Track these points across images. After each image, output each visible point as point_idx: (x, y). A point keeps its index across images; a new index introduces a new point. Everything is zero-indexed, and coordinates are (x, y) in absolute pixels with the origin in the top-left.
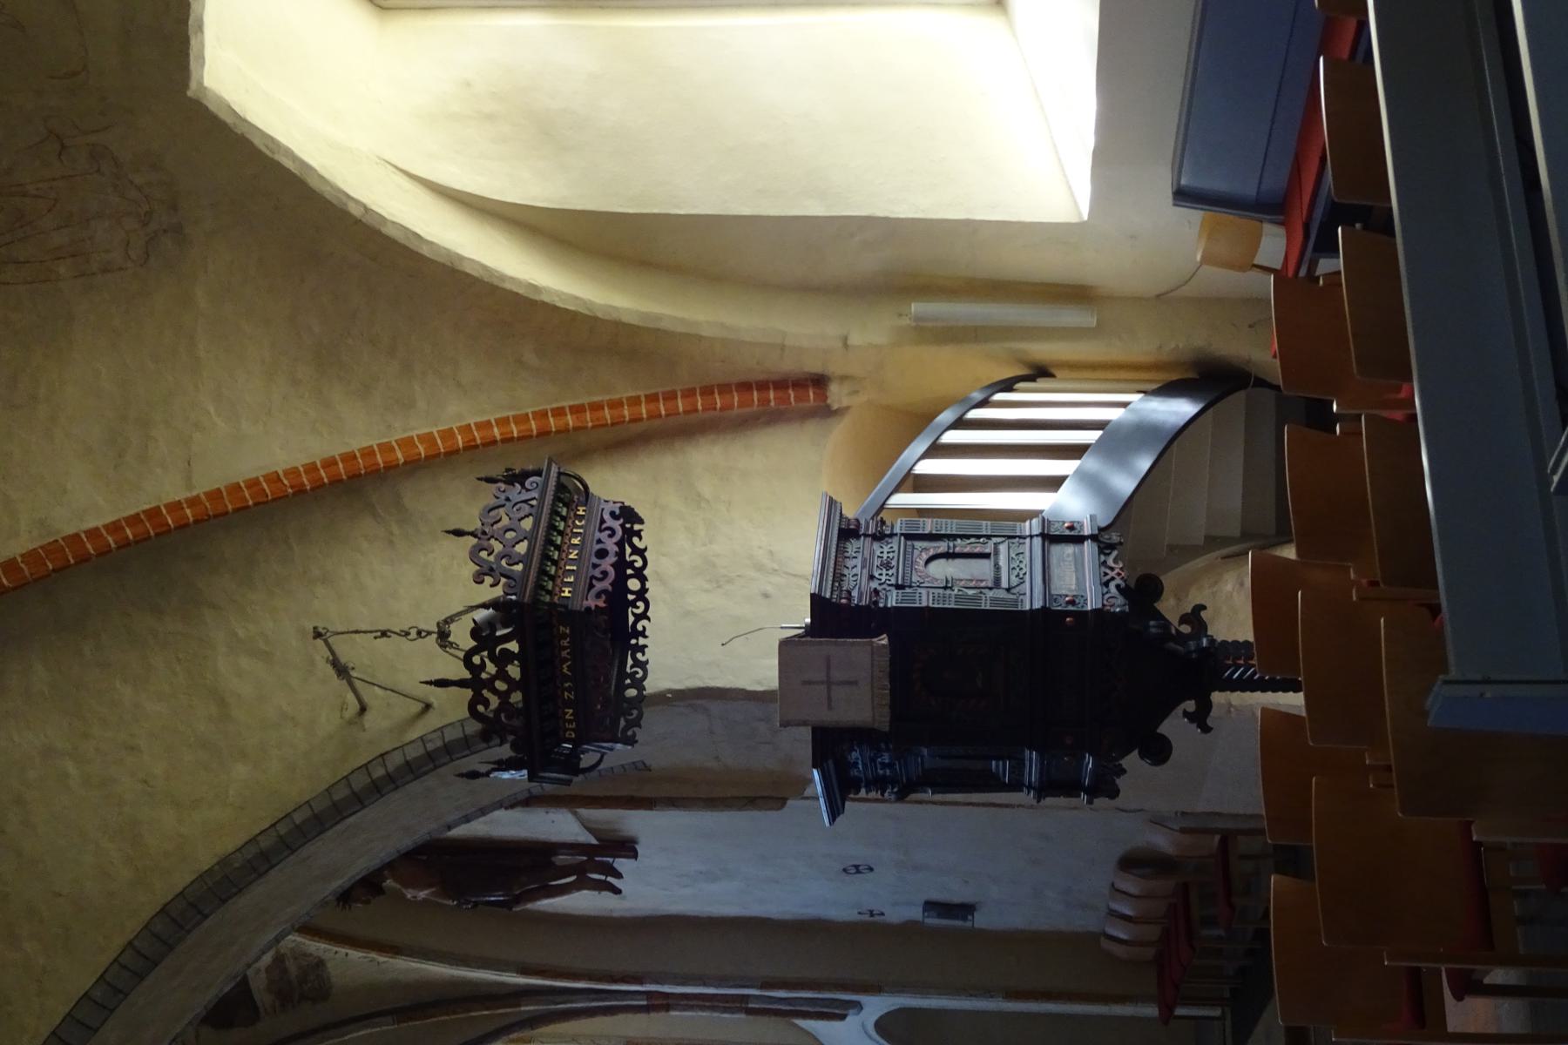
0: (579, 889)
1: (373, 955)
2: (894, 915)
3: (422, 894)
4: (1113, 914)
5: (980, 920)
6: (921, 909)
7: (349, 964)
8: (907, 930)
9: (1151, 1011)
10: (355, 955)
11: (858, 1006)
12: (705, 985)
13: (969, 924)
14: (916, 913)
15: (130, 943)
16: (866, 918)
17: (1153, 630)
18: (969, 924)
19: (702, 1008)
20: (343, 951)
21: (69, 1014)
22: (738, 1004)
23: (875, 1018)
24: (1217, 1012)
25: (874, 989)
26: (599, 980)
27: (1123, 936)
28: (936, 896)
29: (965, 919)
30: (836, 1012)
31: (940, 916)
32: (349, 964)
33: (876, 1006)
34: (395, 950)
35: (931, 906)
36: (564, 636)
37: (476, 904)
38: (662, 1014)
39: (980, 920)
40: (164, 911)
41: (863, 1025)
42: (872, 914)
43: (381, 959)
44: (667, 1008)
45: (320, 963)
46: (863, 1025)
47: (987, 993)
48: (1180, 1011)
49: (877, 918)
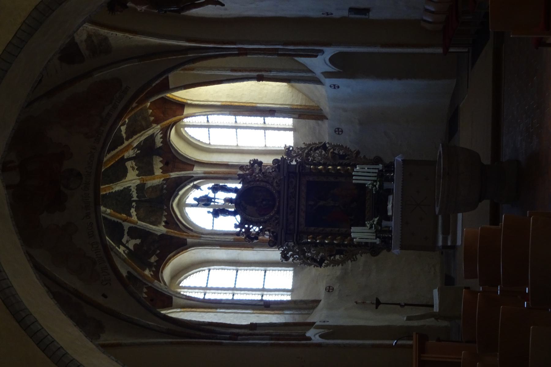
0: (207, 4)
1: (127, 35)
2: (337, 14)
3: (144, 8)
4: (426, 10)
5: (372, 16)
6: (347, 11)
7: (118, 38)
8: (342, 20)
9: (440, 50)
10: (120, 35)
11: (322, 52)
12: (261, 44)
13: (367, 17)
14: (346, 13)
15: (24, 21)
16: (325, 16)
17: (236, 281)
18: (367, 17)
19: (260, 54)
20: (115, 33)
21: (5, 50)
22: (274, 52)
23: (329, 57)
24: (467, 50)
25: (328, 44)
26: (219, 43)
27: (430, 20)
28: (353, 5)
29: (366, 15)
30: (313, 54)
31: (355, 14)
32: (118, 38)
33: (329, 52)
34: (135, 33)
35: (352, 10)
36: (145, 293)
37: (166, 12)
38: (244, 57)
39: (372, 16)
40: (36, 8)
41: (325, 60)
42: (328, 14)
43: (131, 36)
44: (246, 54)
45: (106, 38)
46: (325, 60)
47: (374, 45)
48: (451, 50)
49: (330, 16)
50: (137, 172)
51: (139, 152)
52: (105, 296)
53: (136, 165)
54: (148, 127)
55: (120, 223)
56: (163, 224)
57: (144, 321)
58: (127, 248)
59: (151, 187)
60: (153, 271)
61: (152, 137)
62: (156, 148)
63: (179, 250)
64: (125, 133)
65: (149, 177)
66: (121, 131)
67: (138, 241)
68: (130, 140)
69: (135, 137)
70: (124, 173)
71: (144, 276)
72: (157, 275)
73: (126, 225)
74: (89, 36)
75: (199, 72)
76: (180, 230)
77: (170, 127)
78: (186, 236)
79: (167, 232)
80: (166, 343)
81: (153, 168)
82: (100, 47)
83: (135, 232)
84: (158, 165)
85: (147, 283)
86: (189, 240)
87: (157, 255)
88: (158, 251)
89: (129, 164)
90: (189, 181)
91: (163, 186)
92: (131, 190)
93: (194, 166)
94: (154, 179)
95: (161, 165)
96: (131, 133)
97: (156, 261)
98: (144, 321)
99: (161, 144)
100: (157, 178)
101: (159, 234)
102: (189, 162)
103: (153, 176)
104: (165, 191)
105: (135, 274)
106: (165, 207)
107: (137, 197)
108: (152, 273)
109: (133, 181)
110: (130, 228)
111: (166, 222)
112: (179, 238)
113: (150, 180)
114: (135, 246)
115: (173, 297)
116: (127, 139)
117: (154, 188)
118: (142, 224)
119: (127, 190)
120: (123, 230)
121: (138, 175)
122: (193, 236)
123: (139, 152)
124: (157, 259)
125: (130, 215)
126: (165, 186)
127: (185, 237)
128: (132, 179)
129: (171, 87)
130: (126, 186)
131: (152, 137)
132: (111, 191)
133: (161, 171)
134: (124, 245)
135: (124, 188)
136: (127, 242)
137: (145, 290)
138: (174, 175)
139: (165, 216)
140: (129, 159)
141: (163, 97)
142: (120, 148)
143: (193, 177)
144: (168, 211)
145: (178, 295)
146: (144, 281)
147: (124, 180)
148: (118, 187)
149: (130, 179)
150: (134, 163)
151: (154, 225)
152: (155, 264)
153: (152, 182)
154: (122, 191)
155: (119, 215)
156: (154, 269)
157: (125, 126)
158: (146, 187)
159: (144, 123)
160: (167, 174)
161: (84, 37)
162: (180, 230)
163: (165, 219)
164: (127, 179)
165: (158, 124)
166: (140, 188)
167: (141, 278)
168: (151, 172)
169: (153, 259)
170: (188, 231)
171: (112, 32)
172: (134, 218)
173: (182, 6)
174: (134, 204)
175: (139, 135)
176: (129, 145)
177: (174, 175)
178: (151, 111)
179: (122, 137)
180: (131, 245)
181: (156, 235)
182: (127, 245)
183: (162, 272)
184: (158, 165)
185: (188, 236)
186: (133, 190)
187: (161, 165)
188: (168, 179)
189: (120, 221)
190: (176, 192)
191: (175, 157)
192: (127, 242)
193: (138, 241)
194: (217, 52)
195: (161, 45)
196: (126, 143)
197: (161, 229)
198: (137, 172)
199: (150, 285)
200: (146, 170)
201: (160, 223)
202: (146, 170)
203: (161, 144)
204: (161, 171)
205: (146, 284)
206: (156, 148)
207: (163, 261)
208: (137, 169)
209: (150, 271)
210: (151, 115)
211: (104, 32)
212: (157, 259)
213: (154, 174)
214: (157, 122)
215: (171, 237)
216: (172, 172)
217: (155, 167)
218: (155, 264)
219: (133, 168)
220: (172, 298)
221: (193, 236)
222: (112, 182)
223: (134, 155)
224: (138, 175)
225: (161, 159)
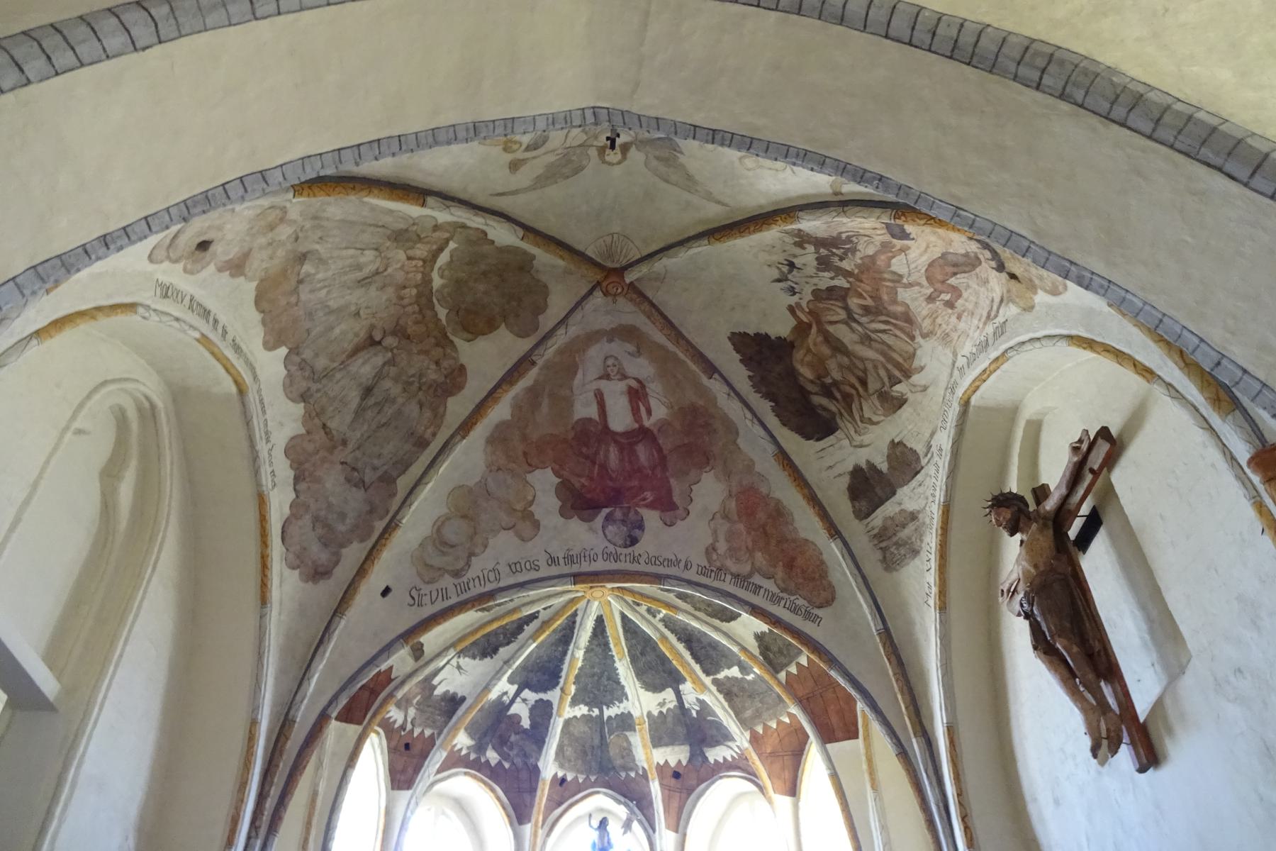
10: (931, 578)
26: (961, 804)
34: (943, 607)
43: (931, 602)
50: (656, 713)
51: (694, 714)
52: (386, 592)
53: (669, 710)
54: (743, 723)
55: (558, 683)
56: (560, 774)
57: (321, 667)
58: (512, 701)
59: (629, 743)
60: (468, 754)
61: (723, 737)
62: (705, 749)
63: (510, 809)
64: (727, 677)
65: (647, 736)
66: (729, 668)
67: (526, 723)
68: (714, 689)
69: (721, 697)
70: (655, 688)
71: (455, 730)
72: (455, 761)
73: (553, 696)
74: (913, 516)
75: (871, 803)
76: (549, 810)
77: (751, 776)
78: (537, 822)
79: (544, 780)
80: (255, 708)
81: (667, 745)
82: (893, 546)
83: (542, 713)
84: (675, 755)
85: (442, 736)
86: (527, 829)
87: (500, 763)
88: (507, 765)
89: (669, 694)
90: (646, 824)
91: (631, 769)
92: (621, 702)
93: (677, 831)
94: (644, 746)
95: (673, 763)
96: (729, 691)
97: (488, 761)
98: (321, 667)
99: (712, 761)
100: (649, 756)
101: (540, 764)
102: (682, 822)
103: (649, 744)
104: (623, 774)
105: (460, 712)
106: (593, 778)
107: (610, 717)
108: (464, 752)
109: (637, 704)
110: (549, 704)
111: (563, 780)
112: (532, 806)
113: (643, 738)
114: (517, 718)
115: (410, 792)
116: (715, 682)
117: (627, 751)
118: (557, 726)
119: (620, 695)
120: (545, 690)
121: (649, 714)
122: (535, 835)
123: (694, 714)
124: (493, 763)
125: (575, 702)
126: (633, 774)
127: (533, 820)
128: (641, 702)
129: (828, 746)
130: (627, 690)
131: (723, 737)
132: (616, 659)
133: (662, 763)
134: (517, 694)
135: (623, 687)
136: (524, 700)
137: (428, 732)
138: (655, 788)
139: (576, 778)
140: (678, 695)
141: (808, 737)
142: (697, 668)
143: (654, 831)
144: (587, 785)
145: (413, 801)
146: (445, 731)
147: (638, 684)
148: (624, 670)
149: (642, 699)
150: (671, 706)
151: (557, 754)
152: (483, 760)
153: (639, 742)
154: (618, 683)
155: (572, 679)
156: (473, 756)
157: (739, 675)
158: (628, 733)
159: (748, 713)
160: (656, 775)
161: (910, 506)
162: (549, 810)
163: (569, 778)
164: (642, 691)
165: (750, 742)
166: (626, 722)
167: (451, 724)
168: (657, 742)
169: (492, 756)
170: (546, 827)
171: (933, 557)
172: (569, 712)
173: (1058, 646)
174: (596, 712)
175: (726, 704)
176: (704, 687)
177: (655, 788)
178: (774, 726)
179: (718, 672)
180: (521, 710)
181: (538, 760)
182: (518, 699)
183: (466, 774)
184: (675, 755)
185: (536, 825)
186: (622, 706)
187: (673, 763)
188: (647, 779)
189: (562, 681)
190: (622, 799)
191: (690, 791)
192: (524, 700)
193: (526, 723)
194: (938, 806)
195: (923, 675)
196: (707, 680)
197: (549, 768)
198: (656, 713)
199: (438, 743)
200: (662, 731)
201: (562, 766)
202: (662, 731)
203: (712, 761)
204: (662, 763)
205: (439, 734)
206: (705, 749)
207: (493, 774)
208: (661, 712)
209: (468, 748)
210: (766, 727)
211: (931, 541)
212: (493, 763)
213: (655, 746)
214: (755, 740)
215: (533, 790)
216: (661, 784)
217: (669, 749)
218: (483, 760)
219: (662, 704)
220: (409, 788)
221: (535, 835)
222: (634, 660)
223: (687, 706)
224: (649, 714)
225: (684, 763)
